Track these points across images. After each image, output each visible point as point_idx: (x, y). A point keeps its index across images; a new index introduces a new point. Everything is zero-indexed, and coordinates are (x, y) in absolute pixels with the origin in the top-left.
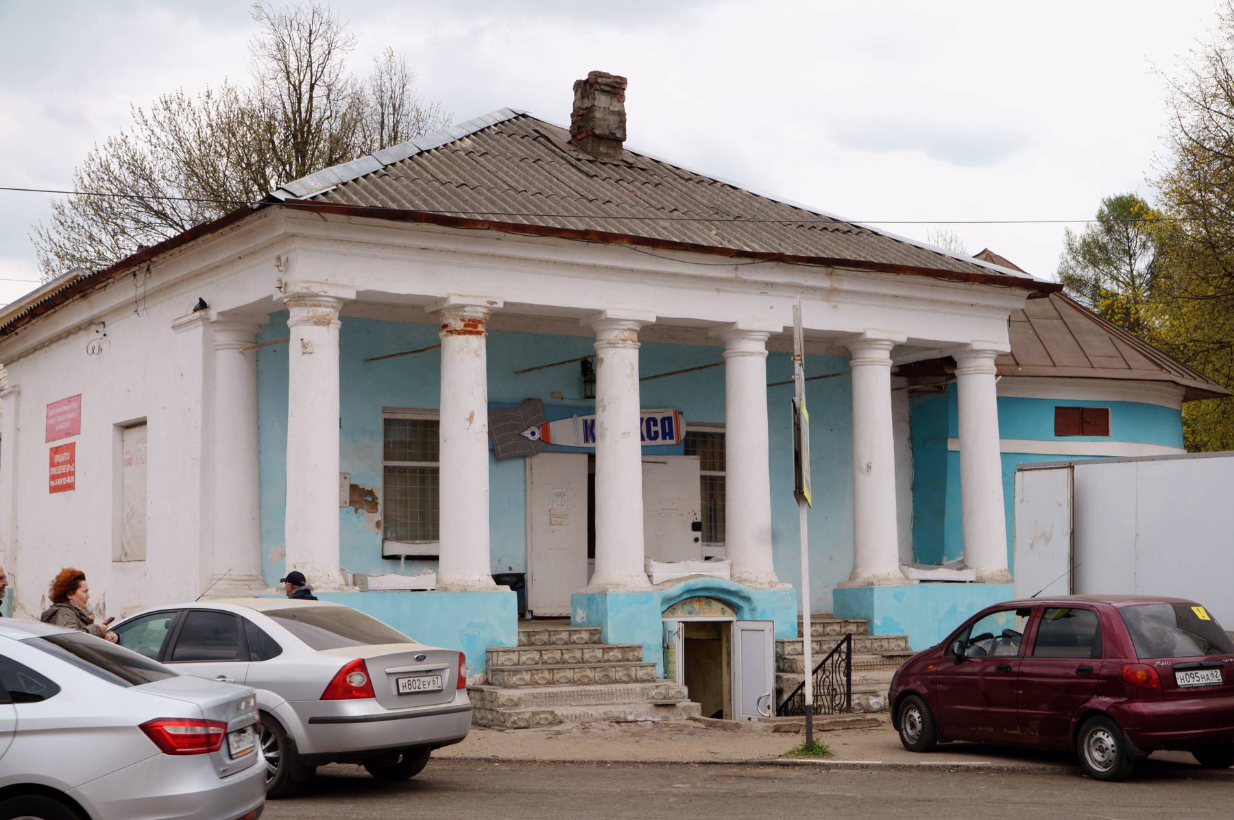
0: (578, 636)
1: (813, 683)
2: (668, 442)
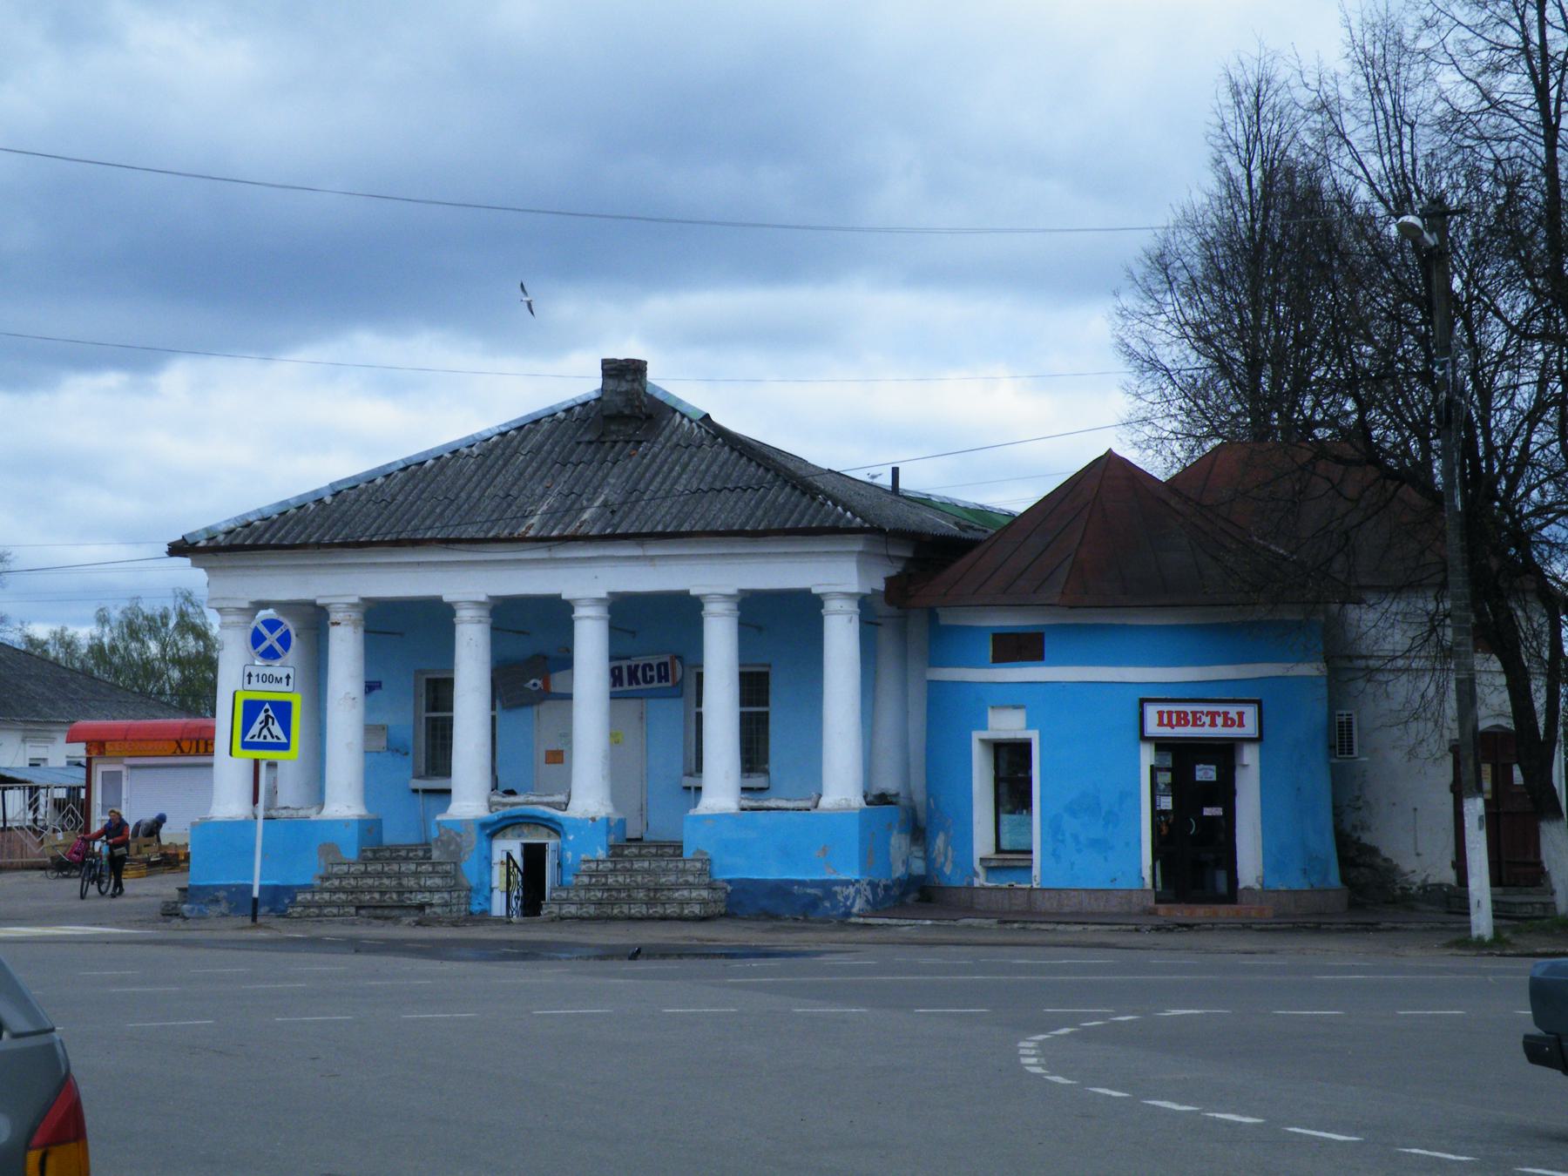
0: (646, 850)
1: (57, 877)
2: (664, 684)
